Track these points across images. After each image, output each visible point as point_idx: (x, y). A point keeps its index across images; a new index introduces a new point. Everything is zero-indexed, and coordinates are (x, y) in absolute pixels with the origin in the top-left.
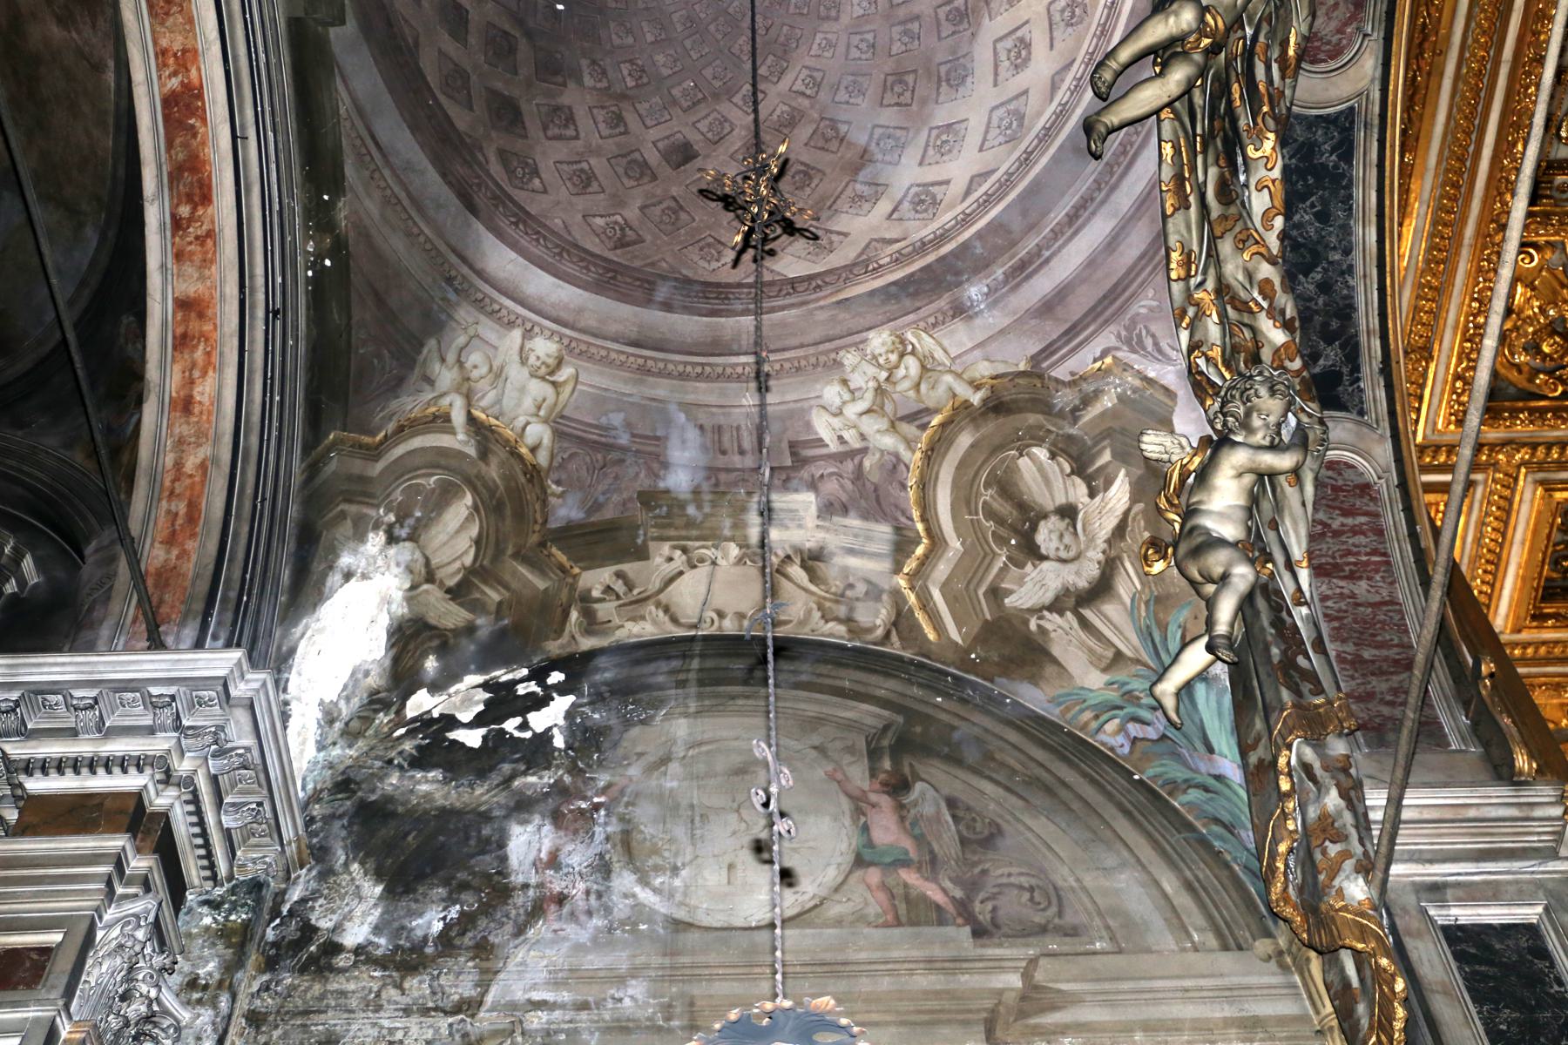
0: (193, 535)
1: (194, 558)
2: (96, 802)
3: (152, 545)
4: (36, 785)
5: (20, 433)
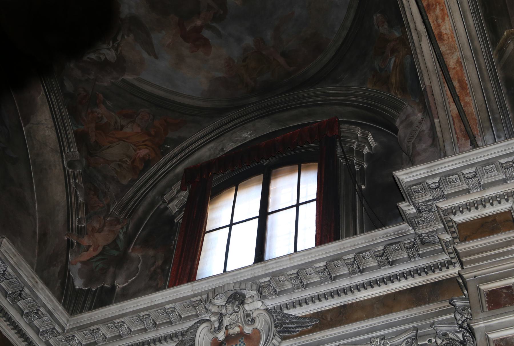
0: (467, 94)
1: (472, 104)
2: (491, 219)
3: (449, 104)
4: (459, 218)
5: (338, 85)
